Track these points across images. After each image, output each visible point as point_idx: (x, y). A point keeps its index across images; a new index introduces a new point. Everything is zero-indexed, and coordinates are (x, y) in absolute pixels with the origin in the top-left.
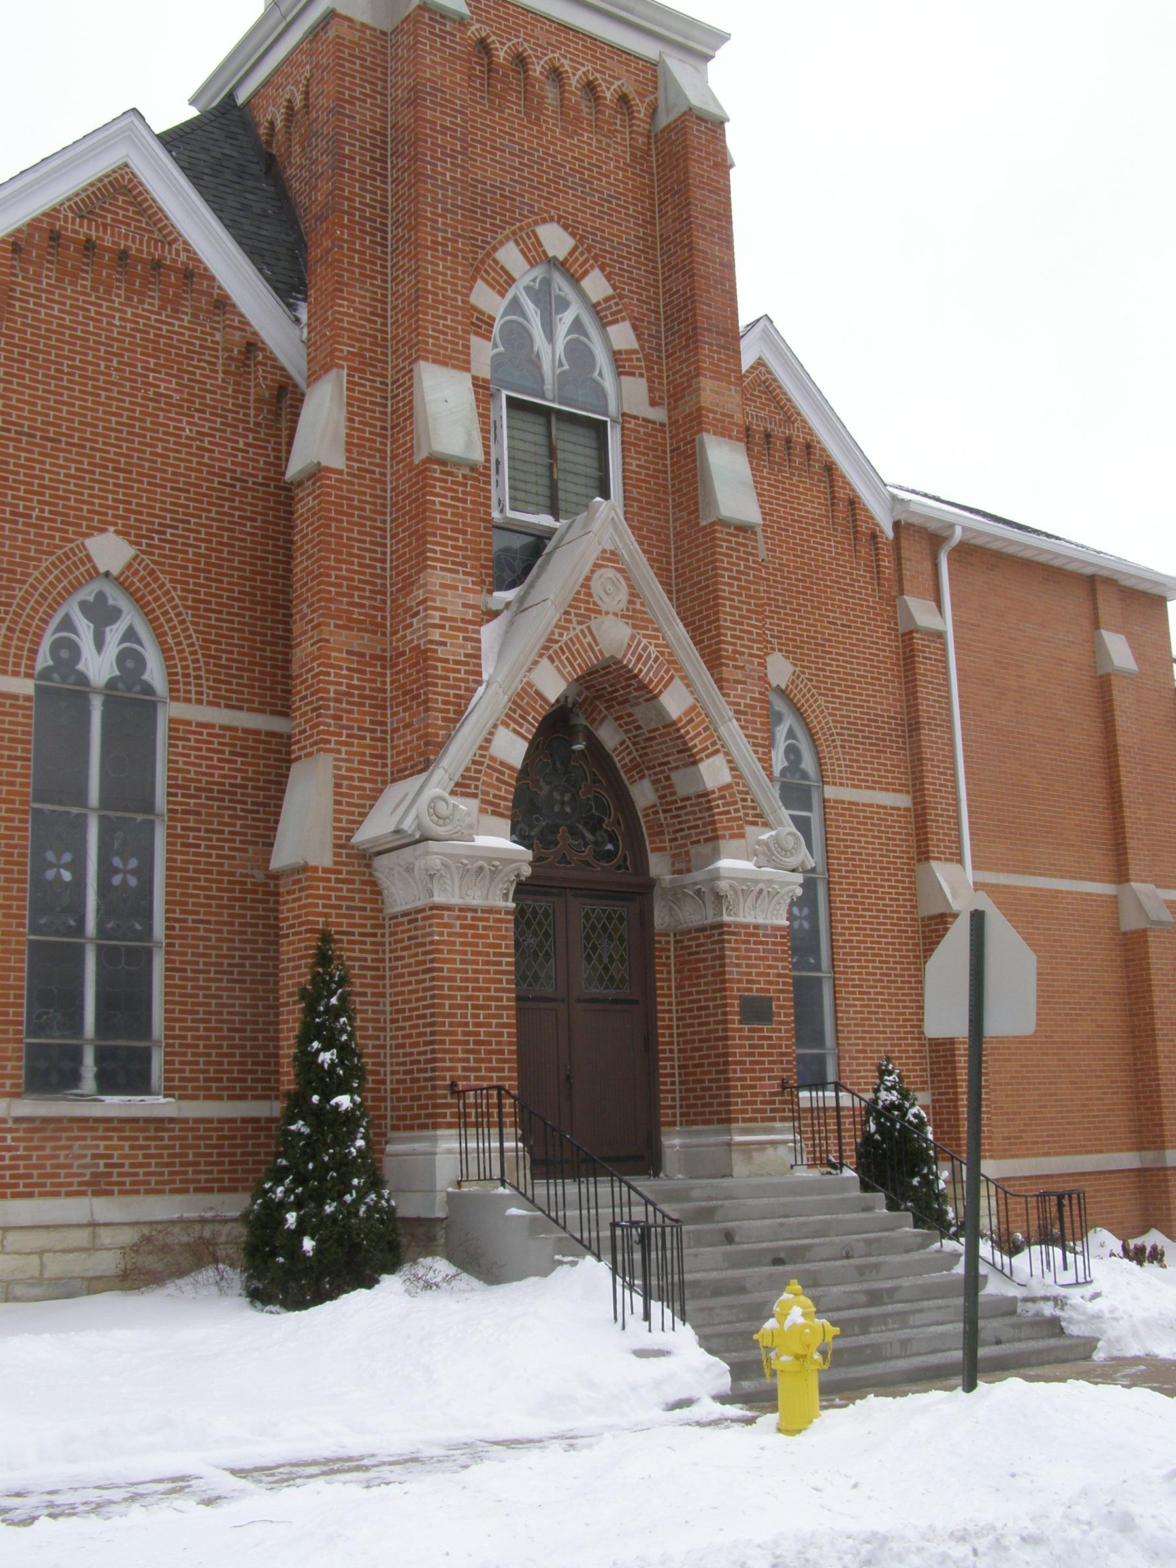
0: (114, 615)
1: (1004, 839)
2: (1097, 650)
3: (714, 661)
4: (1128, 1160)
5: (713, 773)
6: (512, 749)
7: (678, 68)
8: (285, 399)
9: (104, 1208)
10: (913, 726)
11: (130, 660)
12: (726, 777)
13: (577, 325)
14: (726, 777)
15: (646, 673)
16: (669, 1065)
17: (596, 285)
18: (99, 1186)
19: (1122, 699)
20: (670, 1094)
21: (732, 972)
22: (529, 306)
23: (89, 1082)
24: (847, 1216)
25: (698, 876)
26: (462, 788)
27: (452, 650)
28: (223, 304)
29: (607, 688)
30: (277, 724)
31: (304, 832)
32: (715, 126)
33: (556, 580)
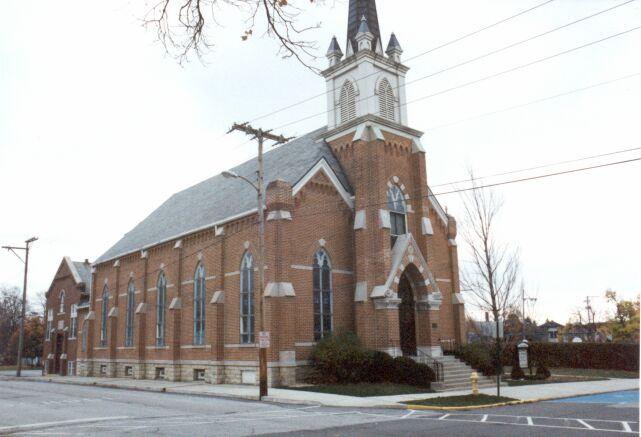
6: (397, 280)
7: (415, 140)
8: (350, 217)
17: (403, 187)
24: (304, 268)
27: (387, 263)
28: (337, 193)
29: (411, 269)
31: (361, 293)
32: (423, 153)
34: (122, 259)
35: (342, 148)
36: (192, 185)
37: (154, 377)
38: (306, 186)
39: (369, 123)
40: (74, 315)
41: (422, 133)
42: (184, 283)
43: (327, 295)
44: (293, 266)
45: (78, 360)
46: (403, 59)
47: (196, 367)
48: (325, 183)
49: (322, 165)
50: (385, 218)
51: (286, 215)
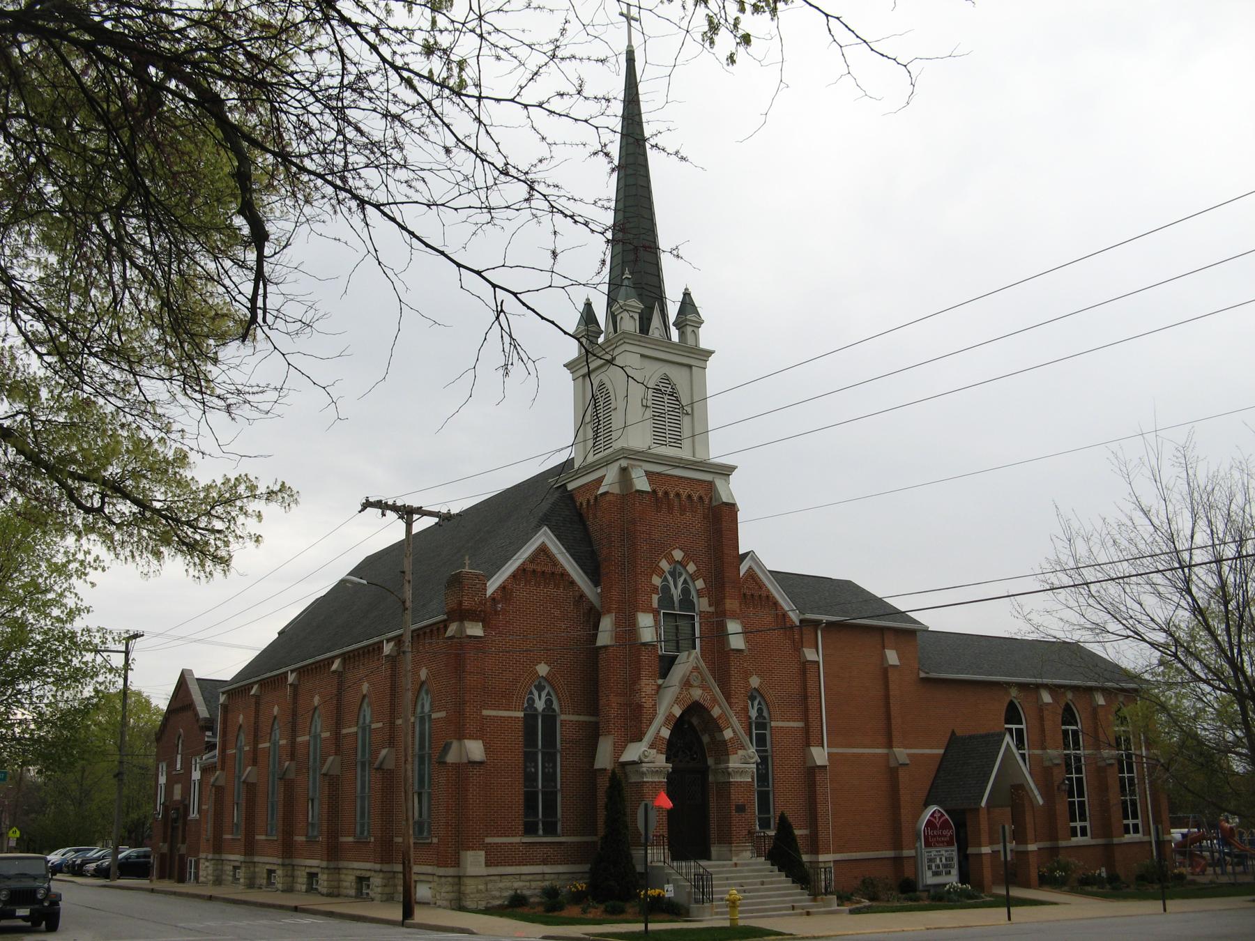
0: (544, 688)
1: (840, 734)
2: (883, 657)
3: (728, 697)
4: (890, 854)
5: (728, 734)
6: (666, 733)
7: (719, 483)
9: (547, 869)
10: (805, 697)
11: (549, 702)
12: (732, 735)
13: (685, 581)
14: (732, 735)
15: (706, 704)
16: (713, 826)
18: (545, 862)
19: (893, 676)
20: (713, 833)
21: (733, 797)
22: (670, 578)
23: (541, 832)
25: (723, 766)
26: (652, 746)
27: (648, 704)
28: (573, 583)
29: (695, 709)
30: (592, 719)
31: (604, 758)
33: (679, 672)
34: (263, 684)
35: (588, 501)
36: (321, 587)
37: (304, 888)
38: (514, 576)
39: (624, 463)
40: (196, 775)
41: (732, 468)
42: (344, 731)
43: (550, 757)
44: (485, 712)
45: (202, 855)
46: (706, 339)
47: (358, 873)
48: (548, 569)
49: (545, 537)
50: (647, 627)
51: (475, 630)
